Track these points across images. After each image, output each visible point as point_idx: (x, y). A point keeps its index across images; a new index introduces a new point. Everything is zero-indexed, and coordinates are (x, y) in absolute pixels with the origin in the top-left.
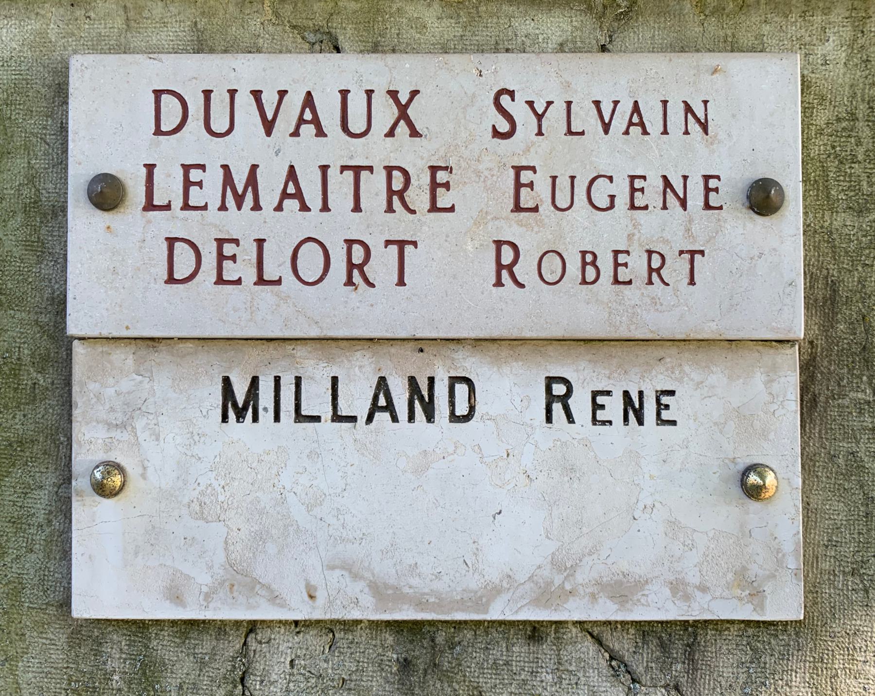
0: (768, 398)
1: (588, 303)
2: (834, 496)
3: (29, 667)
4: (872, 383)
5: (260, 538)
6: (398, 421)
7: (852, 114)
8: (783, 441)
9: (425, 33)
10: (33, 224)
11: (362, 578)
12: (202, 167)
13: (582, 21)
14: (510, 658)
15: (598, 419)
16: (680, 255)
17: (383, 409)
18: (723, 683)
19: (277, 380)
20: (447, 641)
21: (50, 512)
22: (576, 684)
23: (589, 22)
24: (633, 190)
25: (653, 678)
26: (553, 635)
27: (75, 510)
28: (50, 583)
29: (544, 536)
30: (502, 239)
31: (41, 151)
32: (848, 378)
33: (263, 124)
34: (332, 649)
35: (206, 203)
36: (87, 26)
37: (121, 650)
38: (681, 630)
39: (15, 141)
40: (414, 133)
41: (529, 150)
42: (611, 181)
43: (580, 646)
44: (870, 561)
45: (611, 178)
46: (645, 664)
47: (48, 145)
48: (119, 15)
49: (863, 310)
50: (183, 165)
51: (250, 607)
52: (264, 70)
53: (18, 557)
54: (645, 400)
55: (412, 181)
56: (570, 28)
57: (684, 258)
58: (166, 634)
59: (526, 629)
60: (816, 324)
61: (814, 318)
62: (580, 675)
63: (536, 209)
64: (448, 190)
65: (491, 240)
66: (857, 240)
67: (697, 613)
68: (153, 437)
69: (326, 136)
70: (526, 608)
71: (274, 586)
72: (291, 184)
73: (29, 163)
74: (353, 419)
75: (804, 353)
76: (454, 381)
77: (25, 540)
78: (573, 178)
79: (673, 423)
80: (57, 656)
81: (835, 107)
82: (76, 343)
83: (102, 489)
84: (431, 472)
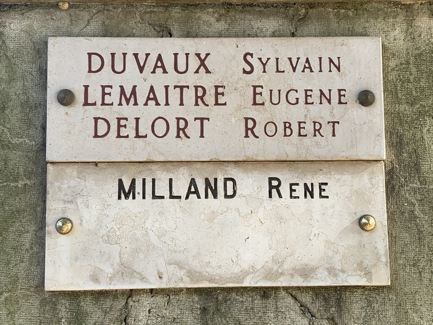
0: (371, 186)
1: (287, 145)
2: (404, 230)
3: (21, 316)
4: (420, 180)
5: (136, 251)
6: (200, 198)
7: (407, 62)
8: (378, 205)
9: (211, 27)
10: (26, 111)
11: (184, 268)
12: (111, 87)
13: (283, 22)
14: (254, 306)
15: (293, 196)
16: (328, 124)
17: (193, 193)
18: (355, 316)
19: (144, 180)
20: (223, 299)
21: (32, 244)
22: (285, 318)
23: (286, 22)
24: (307, 96)
25: (321, 315)
26: (274, 295)
27: (47, 241)
28: (31, 277)
29: (269, 248)
30: (248, 117)
31: (30, 78)
32: (409, 178)
33: (139, 68)
34: (169, 304)
35: (113, 102)
36: (52, 23)
37: (66, 307)
38: (334, 292)
39: (17, 74)
40: (208, 72)
41: (260, 79)
42: (297, 92)
43: (286, 300)
44: (422, 260)
45: (297, 91)
46: (317, 308)
47: (33, 76)
48: (67, 18)
49: (415, 148)
50: (102, 86)
51: (131, 283)
52: (139, 44)
53: (16, 265)
54: (314, 187)
55: (207, 92)
56: (277, 25)
57: (330, 125)
58: (88, 299)
59: (261, 293)
60: (393, 154)
61: (392, 151)
62: (287, 313)
63: (263, 104)
64: (223, 96)
65: (243, 117)
66: (411, 116)
67: (341, 282)
68: (86, 206)
69: (167, 73)
70: (261, 281)
71: (142, 273)
72: (151, 94)
73: (24, 84)
74: (179, 197)
75: (388, 167)
76: (226, 180)
77: (20, 257)
78: (279, 91)
79: (327, 197)
80: (35, 311)
81: (399, 58)
82: (49, 165)
83: (59, 230)
84: (216, 221)
